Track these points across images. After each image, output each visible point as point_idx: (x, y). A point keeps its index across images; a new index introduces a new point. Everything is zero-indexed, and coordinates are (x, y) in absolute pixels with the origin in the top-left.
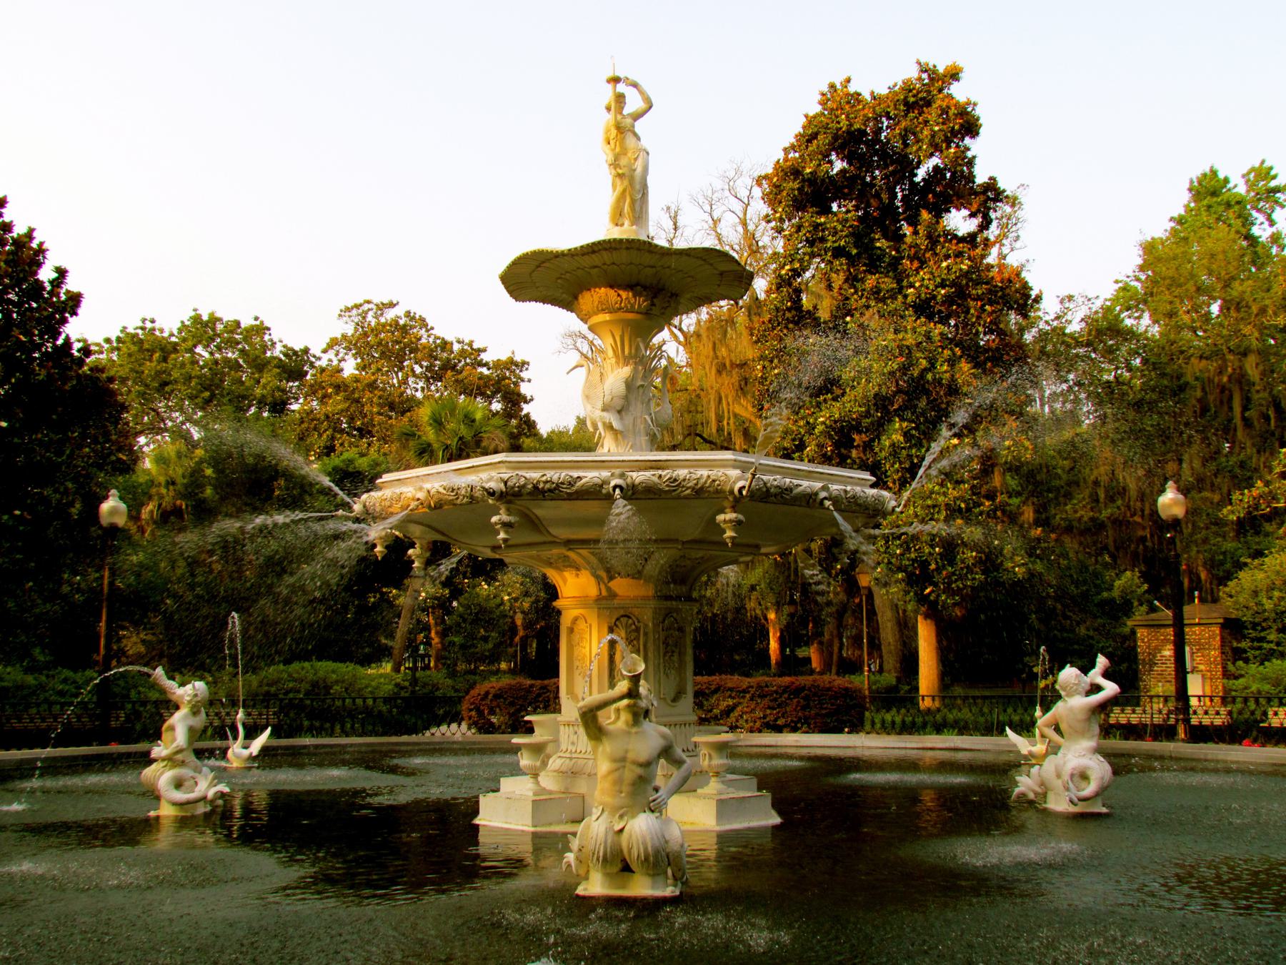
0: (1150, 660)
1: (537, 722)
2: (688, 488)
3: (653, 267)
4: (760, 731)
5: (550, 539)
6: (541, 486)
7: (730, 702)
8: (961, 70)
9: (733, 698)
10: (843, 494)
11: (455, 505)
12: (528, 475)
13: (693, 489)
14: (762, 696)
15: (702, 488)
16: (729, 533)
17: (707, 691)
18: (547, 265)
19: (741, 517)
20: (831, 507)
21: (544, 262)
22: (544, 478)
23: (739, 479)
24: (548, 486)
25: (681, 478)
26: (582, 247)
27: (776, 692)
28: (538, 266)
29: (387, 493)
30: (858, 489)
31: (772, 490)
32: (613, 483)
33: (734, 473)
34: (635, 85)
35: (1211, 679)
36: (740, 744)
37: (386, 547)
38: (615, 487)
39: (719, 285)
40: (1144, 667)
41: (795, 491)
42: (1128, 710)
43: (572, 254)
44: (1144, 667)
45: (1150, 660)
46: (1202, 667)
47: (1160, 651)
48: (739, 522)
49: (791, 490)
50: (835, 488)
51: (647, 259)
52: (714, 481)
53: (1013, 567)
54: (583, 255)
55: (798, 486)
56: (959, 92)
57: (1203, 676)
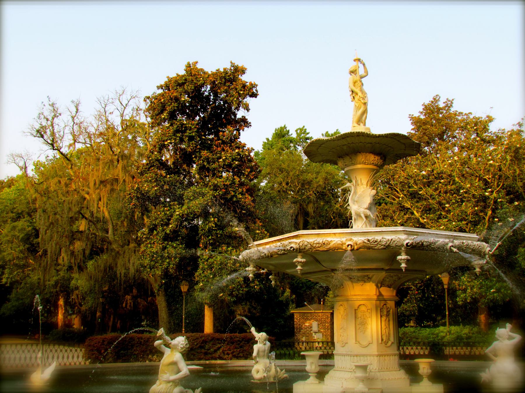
0: (300, 327)
1: (308, 355)
2: (382, 245)
3: (371, 143)
4: (231, 359)
5: (324, 269)
6: (315, 245)
7: (219, 345)
8: (246, 69)
9: (220, 344)
10: (461, 244)
11: (278, 254)
12: (308, 241)
13: (385, 246)
14: (232, 343)
15: (389, 245)
16: (403, 265)
17: (208, 340)
18: (323, 145)
19: (409, 258)
20: (457, 251)
21: (322, 144)
22: (316, 242)
23: (407, 239)
24: (317, 245)
25: (379, 241)
26: (385, 134)
27: (239, 341)
28: (320, 146)
29: (253, 250)
30: (470, 242)
31: (424, 243)
32: (347, 244)
33: (403, 237)
34: (364, 65)
35: (326, 335)
36: (229, 365)
37: (254, 275)
38: (348, 245)
39: (405, 150)
40: (297, 330)
41: (437, 244)
42: (454, 348)
43: (380, 136)
44: (297, 330)
45: (300, 327)
46: (322, 330)
47: (304, 323)
48: (408, 260)
49: (435, 243)
50: (457, 242)
51: (368, 140)
52: (394, 241)
53: (255, 286)
54: (338, 140)
55: (438, 241)
56: (245, 78)
57: (323, 335)
